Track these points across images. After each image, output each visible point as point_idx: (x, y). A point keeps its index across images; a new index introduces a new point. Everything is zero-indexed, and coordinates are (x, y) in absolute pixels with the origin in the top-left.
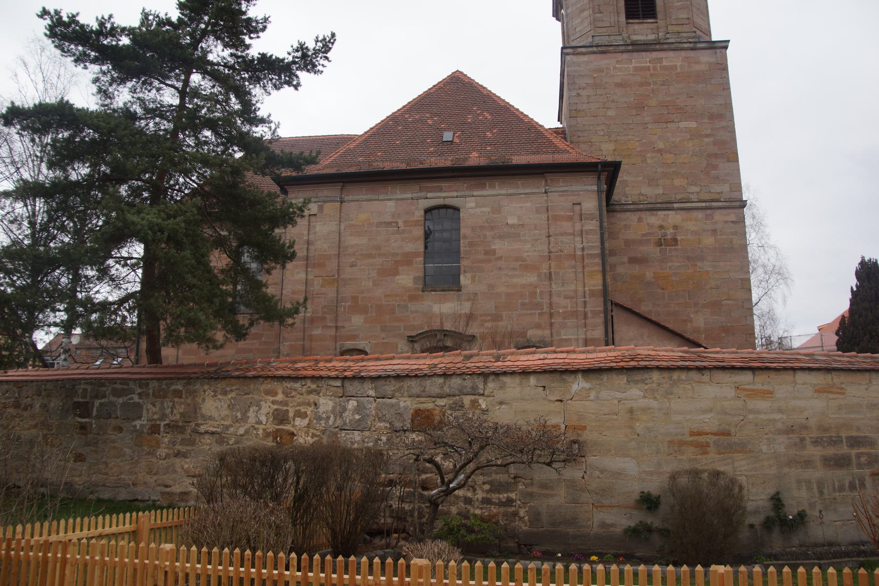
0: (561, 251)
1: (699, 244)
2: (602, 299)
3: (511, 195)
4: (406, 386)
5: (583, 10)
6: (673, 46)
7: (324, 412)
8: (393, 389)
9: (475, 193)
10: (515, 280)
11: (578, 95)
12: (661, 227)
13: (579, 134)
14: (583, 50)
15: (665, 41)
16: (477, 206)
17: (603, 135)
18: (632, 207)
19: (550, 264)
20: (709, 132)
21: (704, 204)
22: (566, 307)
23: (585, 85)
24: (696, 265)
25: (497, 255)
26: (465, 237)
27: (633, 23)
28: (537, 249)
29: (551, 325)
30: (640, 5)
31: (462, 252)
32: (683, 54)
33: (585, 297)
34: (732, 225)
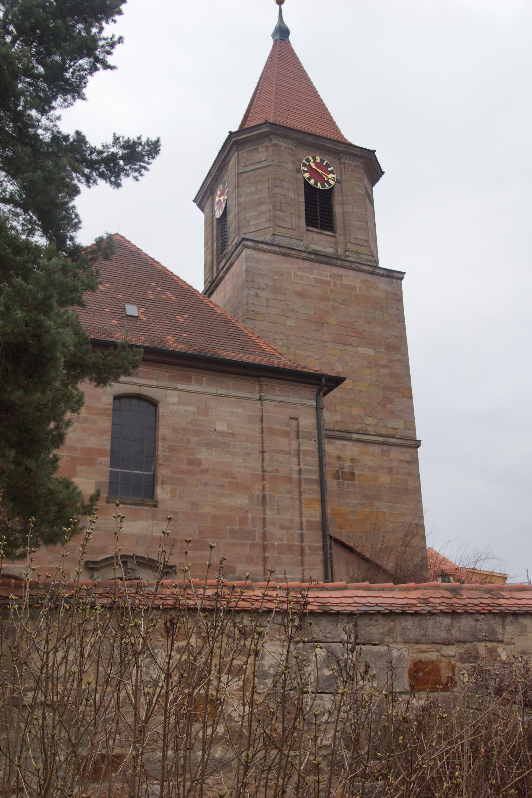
0: (277, 471)
1: (376, 481)
2: (321, 533)
3: (220, 395)
4: (398, 627)
5: (261, 204)
6: (354, 266)
7: (271, 666)
8: (381, 631)
9: (179, 386)
10: (223, 501)
11: (257, 295)
14: (265, 247)
15: (345, 258)
16: (180, 403)
17: (282, 346)
19: (264, 486)
20: (385, 362)
21: (381, 439)
22: (282, 540)
23: (265, 287)
24: (372, 505)
25: (203, 467)
26: (164, 439)
27: (312, 231)
29: (265, 559)
30: (318, 214)
31: (160, 457)
32: (362, 276)
33: (301, 529)
34: (406, 465)
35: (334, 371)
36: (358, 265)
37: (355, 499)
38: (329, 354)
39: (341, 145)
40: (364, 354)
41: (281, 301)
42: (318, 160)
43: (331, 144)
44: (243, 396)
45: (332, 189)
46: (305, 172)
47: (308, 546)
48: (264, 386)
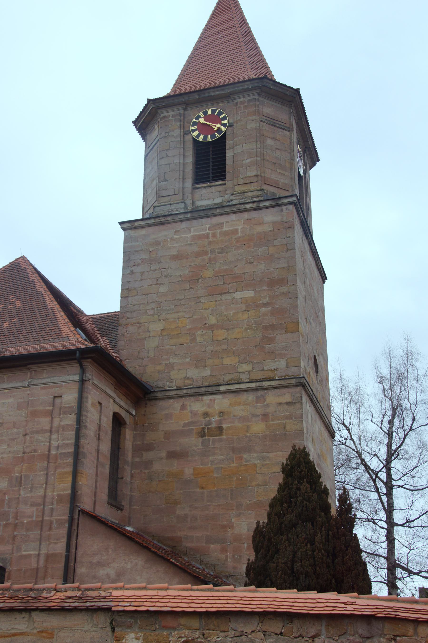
1: (247, 432)
12: (206, 414)
13: (129, 315)
17: (153, 315)
18: (174, 393)
21: (253, 385)
23: (140, 261)
24: (241, 458)
28: (12, 450)
32: (246, 215)
34: (286, 407)
35: (207, 325)
36: (239, 206)
37: (221, 455)
38: (202, 309)
39: (227, 87)
40: (241, 298)
41: (156, 270)
42: (209, 112)
43: (217, 91)
44: (13, 386)
45: (224, 137)
46: (194, 131)
47: (56, 520)
48: (33, 372)
